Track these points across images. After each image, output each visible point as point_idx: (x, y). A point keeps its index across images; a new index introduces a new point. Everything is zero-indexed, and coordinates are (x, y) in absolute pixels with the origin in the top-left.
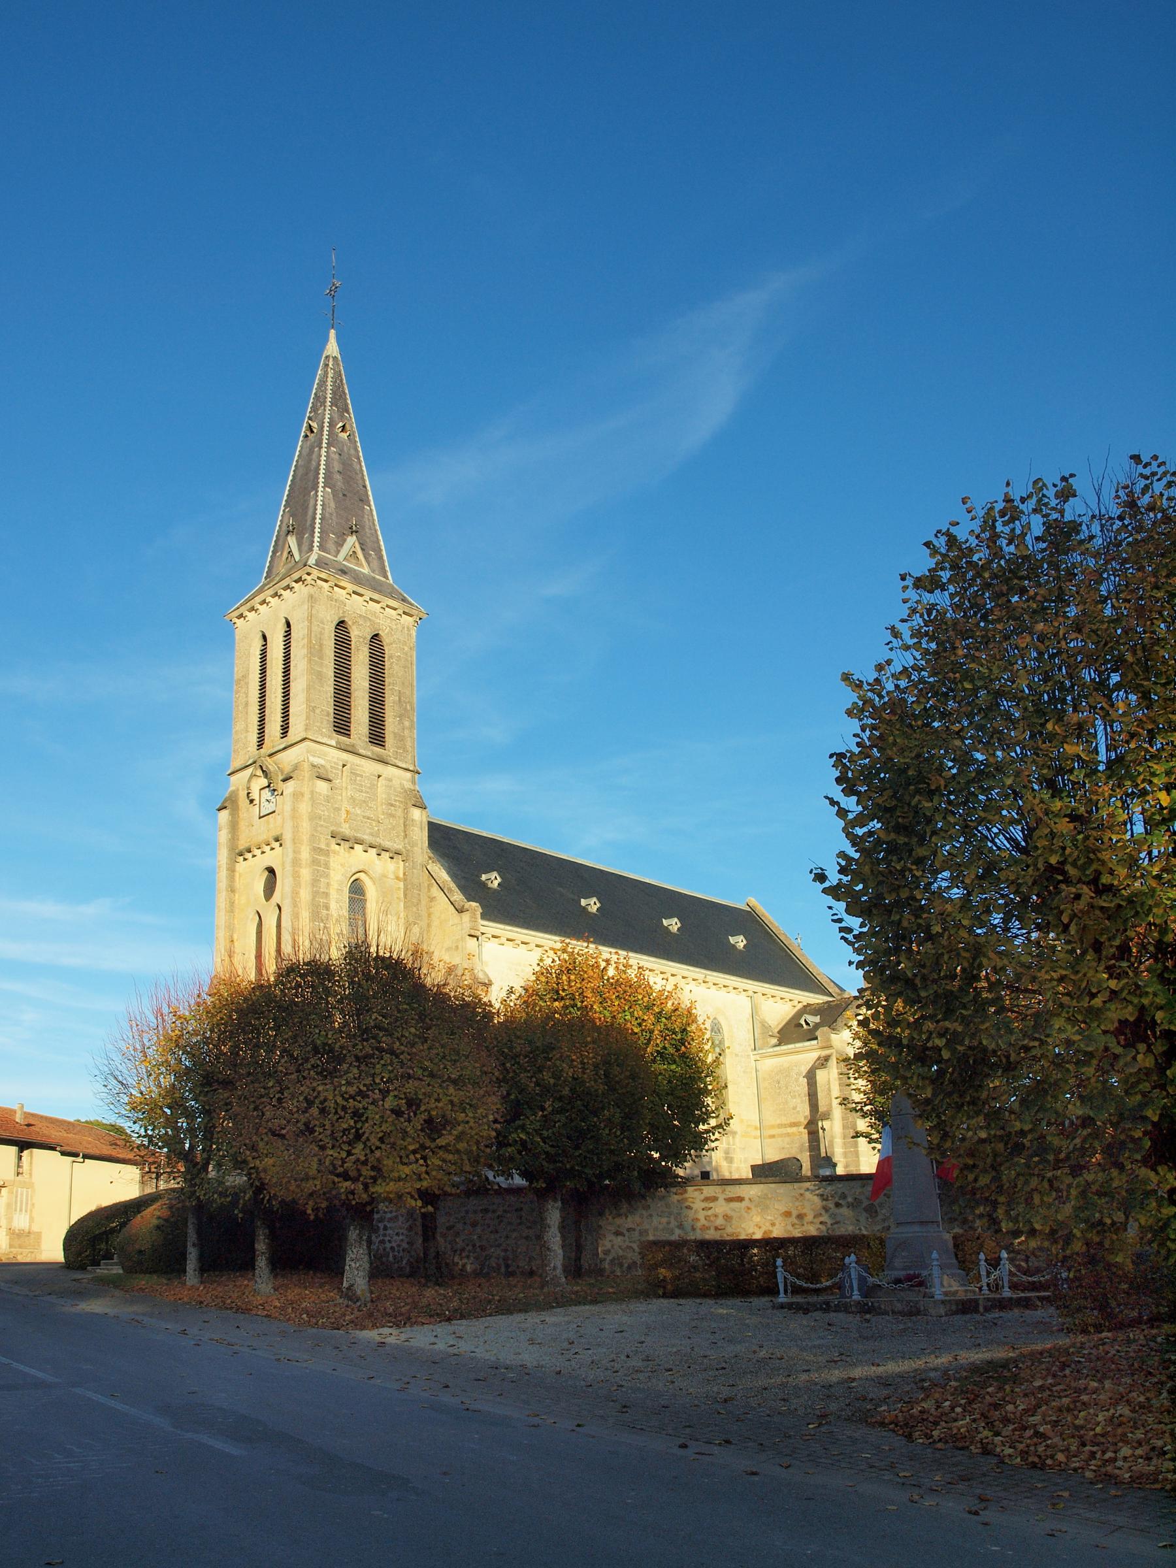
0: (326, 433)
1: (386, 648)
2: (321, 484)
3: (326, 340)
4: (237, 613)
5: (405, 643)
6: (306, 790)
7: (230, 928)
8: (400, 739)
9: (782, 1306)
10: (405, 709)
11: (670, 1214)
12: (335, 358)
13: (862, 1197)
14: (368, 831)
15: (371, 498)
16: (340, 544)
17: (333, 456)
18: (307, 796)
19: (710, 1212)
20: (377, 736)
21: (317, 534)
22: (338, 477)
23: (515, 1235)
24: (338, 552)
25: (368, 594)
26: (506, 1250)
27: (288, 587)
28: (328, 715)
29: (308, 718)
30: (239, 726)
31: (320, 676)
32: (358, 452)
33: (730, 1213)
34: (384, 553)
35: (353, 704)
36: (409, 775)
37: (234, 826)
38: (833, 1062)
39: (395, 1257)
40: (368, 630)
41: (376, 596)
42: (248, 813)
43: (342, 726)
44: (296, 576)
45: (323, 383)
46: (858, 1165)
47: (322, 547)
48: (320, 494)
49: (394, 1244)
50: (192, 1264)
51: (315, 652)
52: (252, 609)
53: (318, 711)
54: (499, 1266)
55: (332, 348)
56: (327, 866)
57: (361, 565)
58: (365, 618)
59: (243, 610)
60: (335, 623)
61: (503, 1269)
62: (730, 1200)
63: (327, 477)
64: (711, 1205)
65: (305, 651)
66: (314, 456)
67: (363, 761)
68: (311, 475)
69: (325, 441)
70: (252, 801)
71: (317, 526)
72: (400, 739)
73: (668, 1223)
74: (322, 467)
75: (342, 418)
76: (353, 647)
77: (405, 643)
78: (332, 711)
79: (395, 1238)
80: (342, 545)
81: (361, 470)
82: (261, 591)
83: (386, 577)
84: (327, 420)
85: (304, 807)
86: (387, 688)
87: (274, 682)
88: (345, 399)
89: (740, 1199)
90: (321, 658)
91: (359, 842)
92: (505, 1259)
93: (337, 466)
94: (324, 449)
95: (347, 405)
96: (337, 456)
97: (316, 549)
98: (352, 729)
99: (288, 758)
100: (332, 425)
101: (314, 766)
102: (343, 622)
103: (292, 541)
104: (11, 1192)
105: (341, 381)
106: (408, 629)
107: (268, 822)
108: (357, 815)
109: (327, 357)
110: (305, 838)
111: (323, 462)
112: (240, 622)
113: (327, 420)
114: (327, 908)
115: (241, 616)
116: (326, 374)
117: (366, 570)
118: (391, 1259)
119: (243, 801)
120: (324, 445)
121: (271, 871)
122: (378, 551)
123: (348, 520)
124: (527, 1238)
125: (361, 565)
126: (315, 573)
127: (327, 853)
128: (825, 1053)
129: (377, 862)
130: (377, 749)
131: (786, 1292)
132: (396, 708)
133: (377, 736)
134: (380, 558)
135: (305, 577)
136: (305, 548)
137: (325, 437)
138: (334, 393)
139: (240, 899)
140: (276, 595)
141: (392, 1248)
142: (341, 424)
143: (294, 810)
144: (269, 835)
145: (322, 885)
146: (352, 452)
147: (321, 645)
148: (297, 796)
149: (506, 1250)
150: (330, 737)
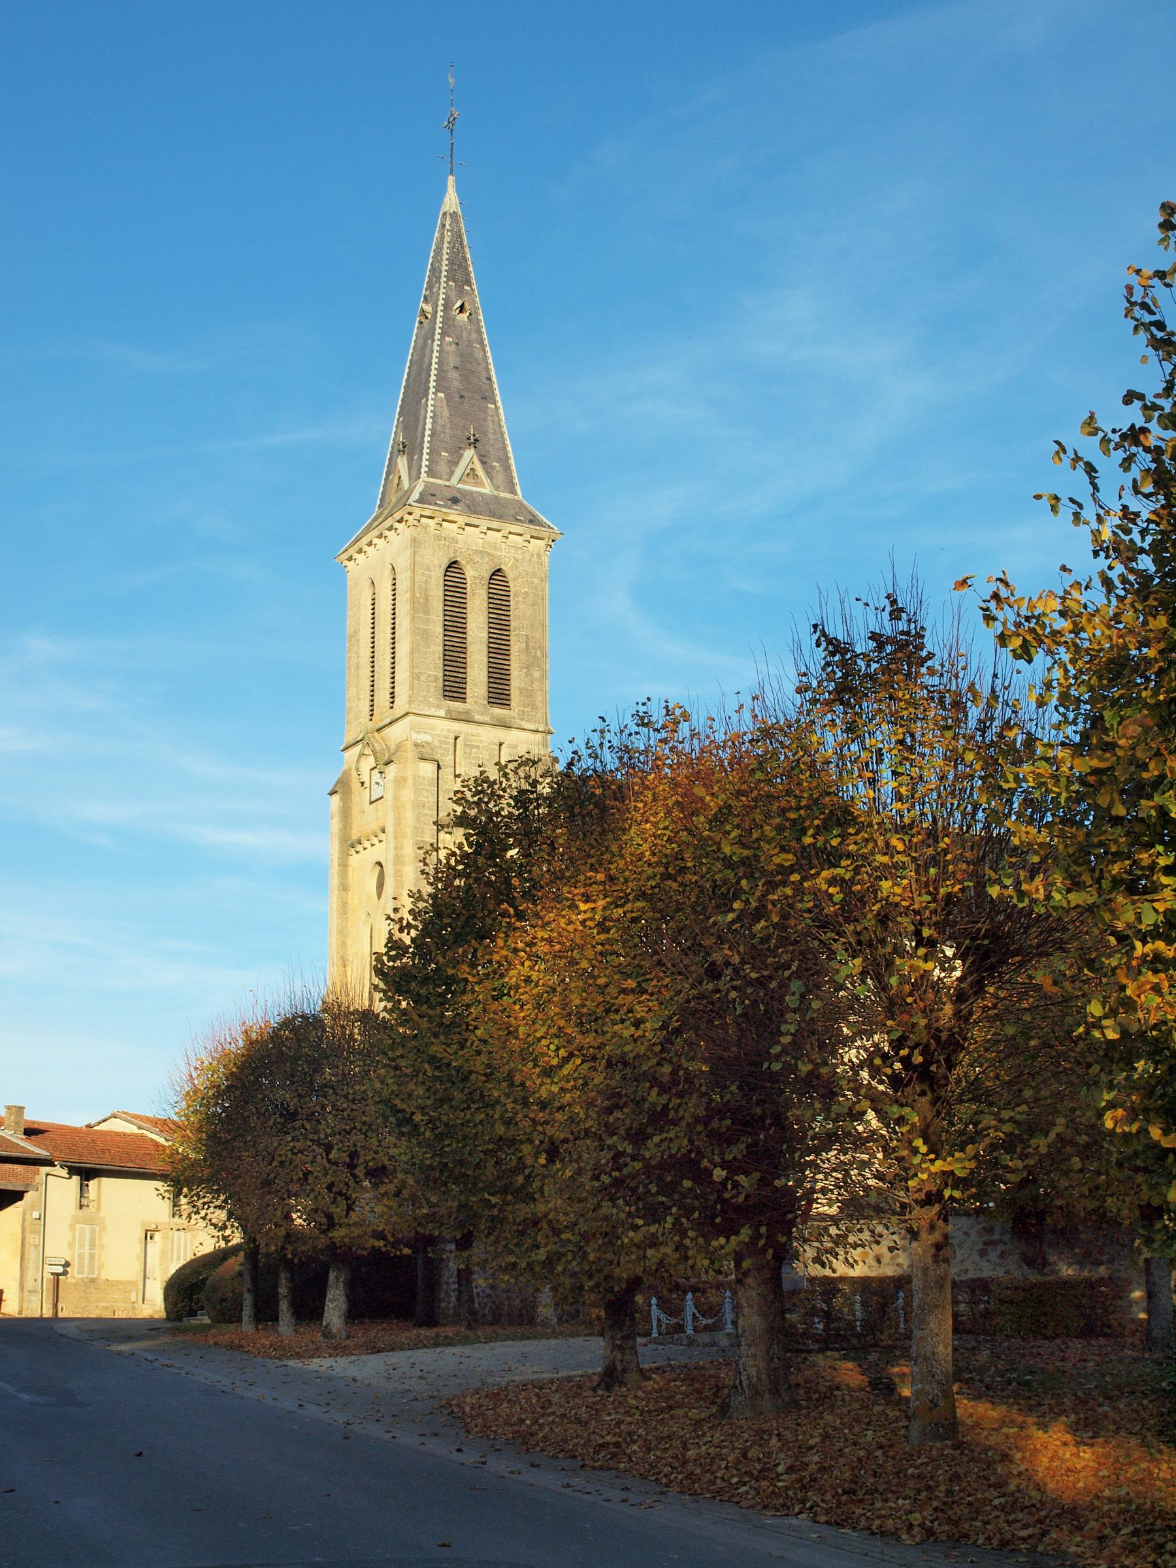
0: (439, 319)
1: (511, 584)
2: (432, 390)
3: (444, 190)
4: (345, 556)
5: (534, 575)
6: (409, 774)
7: (343, 933)
8: (528, 694)
10: (535, 657)
12: (454, 215)
15: (497, 392)
16: (454, 463)
17: (448, 348)
18: (410, 781)
20: (499, 694)
21: (425, 457)
22: (454, 375)
24: (452, 473)
25: (484, 523)
27: (390, 529)
28: (436, 680)
29: (412, 687)
30: (351, 693)
31: (426, 634)
32: (480, 333)
34: (512, 461)
35: (468, 660)
36: (539, 737)
37: (346, 813)
41: (495, 524)
42: (360, 798)
43: (454, 688)
44: (397, 516)
45: (439, 250)
47: (431, 473)
48: (430, 402)
50: (247, 1311)
51: (420, 606)
52: (360, 551)
53: (423, 678)
55: (451, 201)
57: (482, 484)
58: (482, 553)
59: (352, 551)
60: (444, 566)
63: (440, 378)
66: (427, 351)
67: (480, 730)
68: (424, 375)
69: (438, 331)
70: (362, 783)
71: (426, 445)
72: (528, 694)
74: (434, 366)
75: (461, 293)
76: (468, 591)
77: (534, 575)
80: (456, 464)
81: (486, 357)
82: (367, 531)
83: (514, 492)
84: (441, 302)
85: (408, 795)
86: (512, 633)
88: (466, 268)
90: (427, 613)
93: (452, 361)
94: (437, 343)
95: (467, 274)
96: (453, 348)
97: (423, 475)
98: (468, 691)
99: (395, 733)
100: (447, 306)
101: (417, 745)
102: (455, 562)
103: (402, 463)
104: (165, 1237)
105: (461, 243)
106: (539, 555)
107: (377, 809)
109: (444, 214)
110: (409, 830)
111: (435, 360)
112: (350, 564)
113: (441, 302)
115: (350, 559)
116: (442, 237)
117: (487, 489)
119: (355, 785)
120: (437, 337)
121: (379, 864)
122: (504, 461)
123: (466, 428)
125: (482, 484)
126: (417, 512)
130: (499, 711)
132: (523, 657)
133: (499, 694)
134: (507, 468)
135: (406, 517)
136: (414, 473)
137: (439, 325)
138: (451, 262)
139: (353, 898)
140: (380, 536)
142: (459, 304)
143: (396, 798)
144: (374, 826)
146: (474, 336)
147: (427, 598)
148: (400, 782)
150: (439, 707)
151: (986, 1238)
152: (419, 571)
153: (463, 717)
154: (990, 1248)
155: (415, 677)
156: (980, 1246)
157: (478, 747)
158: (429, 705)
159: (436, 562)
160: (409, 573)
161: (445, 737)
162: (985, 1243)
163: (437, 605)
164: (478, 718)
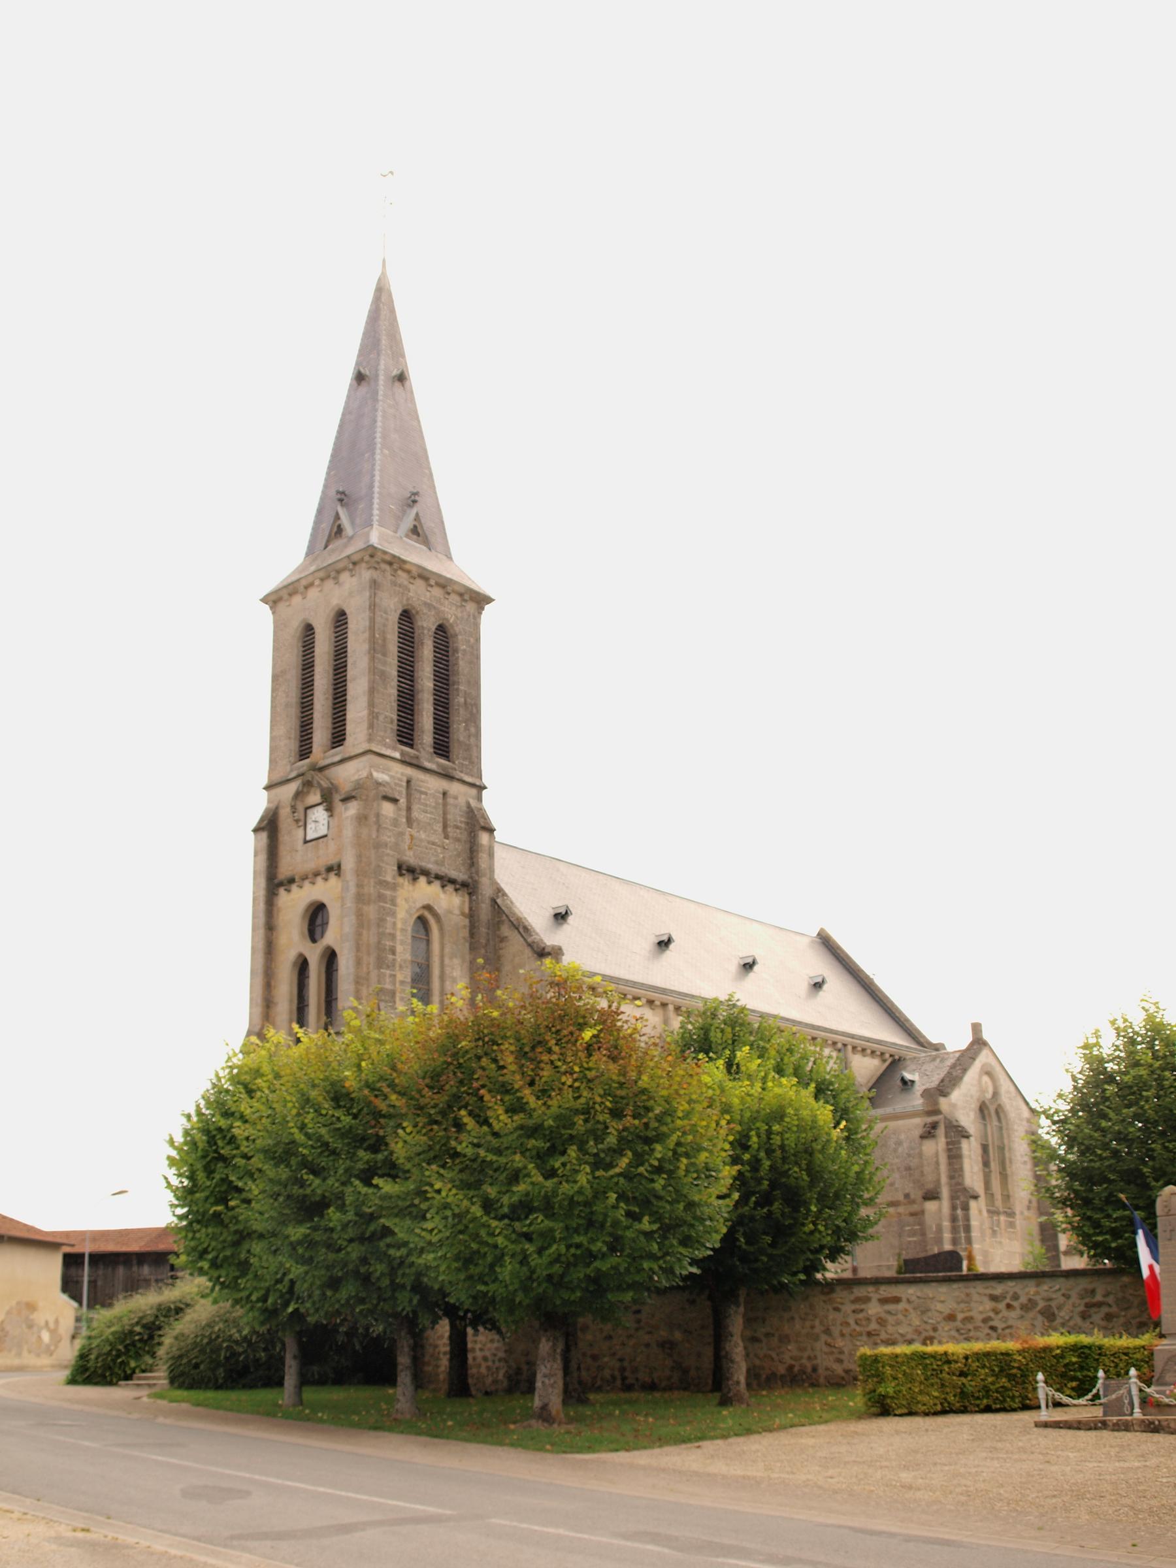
2: (379, 446)
9: (1046, 1425)
11: (815, 1316)
13: (1037, 1298)
14: (433, 859)
19: (861, 1316)
23: (632, 1342)
26: (621, 1360)
28: (392, 722)
31: (383, 675)
33: (883, 1315)
38: (941, 1131)
39: (488, 1368)
40: (433, 619)
46: (1059, 1266)
48: (378, 457)
49: (487, 1353)
51: (376, 648)
53: (381, 718)
54: (613, 1377)
56: (393, 902)
60: (399, 612)
61: (618, 1383)
62: (884, 1301)
64: (863, 1306)
65: (366, 646)
73: (812, 1327)
78: (395, 717)
79: (489, 1345)
87: (325, 681)
89: (897, 1300)
90: (384, 655)
91: (426, 873)
92: (623, 1369)
108: (421, 840)
114: (394, 953)
118: (483, 1370)
124: (647, 1345)
127: (394, 887)
128: (930, 1119)
129: (442, 896)
131: (1047, 1406)
133: (442, 748)
141: (485, 1359)
145: (389, 925)
147: (384, 640)
149: (621, 1360)
150: (394, 749)
151: (1087, 1300)
152: (378, 613)
153: (414, 762)
154: (1093, 1310)
155: (373, 716)
156: (1082, 1308)
157: (426, 794)
158: (385, 745)
159: (392, 606)
160: (368, 613)
161: (400, 780)
162: (1087, 1305)
163: (393, 647)
164: (428, 765)
